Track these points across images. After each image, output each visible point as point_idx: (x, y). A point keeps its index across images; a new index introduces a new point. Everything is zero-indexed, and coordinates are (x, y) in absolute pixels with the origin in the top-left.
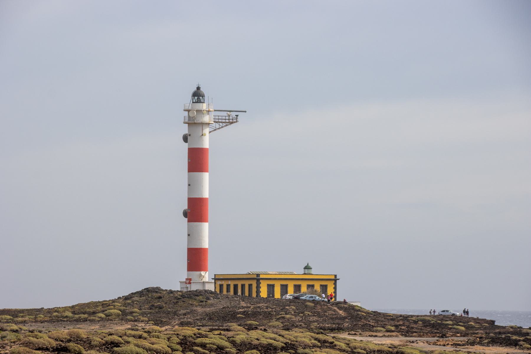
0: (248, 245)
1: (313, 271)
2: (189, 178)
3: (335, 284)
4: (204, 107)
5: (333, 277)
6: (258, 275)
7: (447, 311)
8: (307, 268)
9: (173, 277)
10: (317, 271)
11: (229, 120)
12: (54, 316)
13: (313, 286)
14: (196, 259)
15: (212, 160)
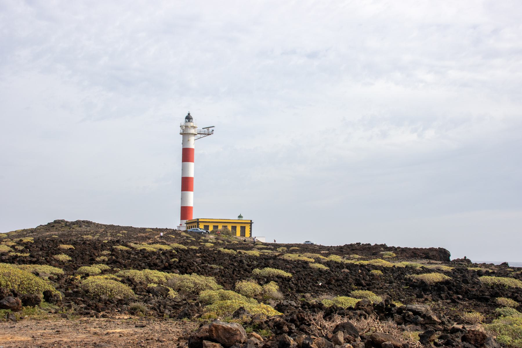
0: (207, 208)
1: (243, 219)
2: (182, 194)
3: (251, 226)
4: (192, 124)
5: (250, 222)
6: (198, 219)
7: (308, 242)
8: (240, 217)
9: (174, 222)
10: (246, 218)
11: (208, 132)
12: (331, 250)
13: (226, 226)
14: (185, 212)
15: (196, 155)
